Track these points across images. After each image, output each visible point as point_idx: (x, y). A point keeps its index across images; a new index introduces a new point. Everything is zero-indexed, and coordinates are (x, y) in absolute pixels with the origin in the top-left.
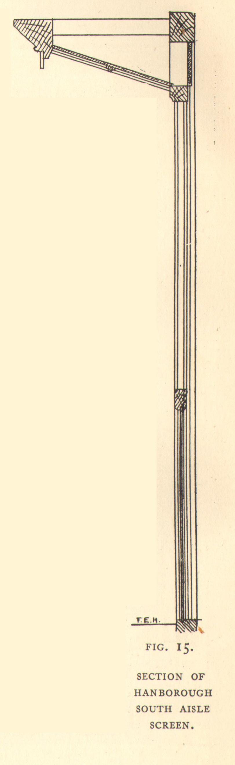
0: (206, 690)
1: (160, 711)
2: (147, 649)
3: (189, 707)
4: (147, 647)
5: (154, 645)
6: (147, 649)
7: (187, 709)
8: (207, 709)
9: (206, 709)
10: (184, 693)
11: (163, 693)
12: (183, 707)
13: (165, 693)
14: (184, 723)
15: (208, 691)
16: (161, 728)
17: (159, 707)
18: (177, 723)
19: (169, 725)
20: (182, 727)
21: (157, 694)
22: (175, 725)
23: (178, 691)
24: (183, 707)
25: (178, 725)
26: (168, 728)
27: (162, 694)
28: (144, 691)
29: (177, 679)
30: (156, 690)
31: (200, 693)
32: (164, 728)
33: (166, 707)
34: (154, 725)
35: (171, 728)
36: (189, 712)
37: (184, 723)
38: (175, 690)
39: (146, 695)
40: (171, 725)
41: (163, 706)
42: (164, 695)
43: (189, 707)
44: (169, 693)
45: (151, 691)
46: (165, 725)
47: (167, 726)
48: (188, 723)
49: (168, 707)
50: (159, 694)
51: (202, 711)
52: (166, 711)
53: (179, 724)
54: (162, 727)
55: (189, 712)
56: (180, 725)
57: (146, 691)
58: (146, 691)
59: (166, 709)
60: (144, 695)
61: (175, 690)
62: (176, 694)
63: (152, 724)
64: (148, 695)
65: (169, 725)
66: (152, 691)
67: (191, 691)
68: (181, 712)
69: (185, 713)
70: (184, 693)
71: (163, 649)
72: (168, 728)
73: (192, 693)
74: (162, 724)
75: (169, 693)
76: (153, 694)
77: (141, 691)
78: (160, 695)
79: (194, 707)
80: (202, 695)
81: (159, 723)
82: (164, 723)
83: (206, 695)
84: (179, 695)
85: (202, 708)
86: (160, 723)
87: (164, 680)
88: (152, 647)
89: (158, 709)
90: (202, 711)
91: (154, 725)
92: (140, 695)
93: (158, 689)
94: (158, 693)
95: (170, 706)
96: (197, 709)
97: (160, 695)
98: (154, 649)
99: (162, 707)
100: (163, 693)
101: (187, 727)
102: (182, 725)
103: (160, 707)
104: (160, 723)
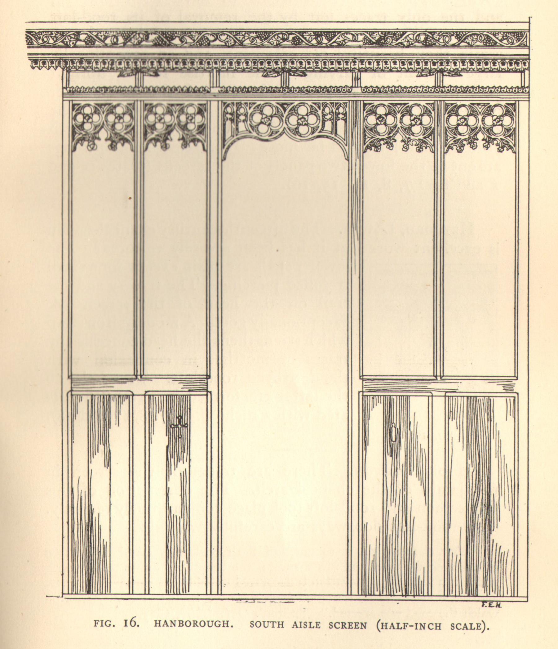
0: (224, 621)
1: (273, 627)
2: (95, 626)
3: (301, 622)
4: (95, 623)
5: (102, 621)
6: (95, 626)
7: (299, 625)
10: (202, 624)
11: (182, 623)
12: (295, 623)
13: (184, 623)
14: (362, 624)
15: (226, 622)
16: (339, 628)
17: (272, 623)
18: (355, 623)
19: (347, 626)
20: (360, 627)
21: (176, 625)
22: (353, 625)
23: (197, 622)
24: (295, 623)
25: (356, 625)
27: (181, 625)
28: (391, 624)
29: (425, 624)
30: (175, 621)
31: (217, 624)
32: (342, 628)
33: (279, 622)
34: (333, 625)
35: (349, 628)
36: (301, 627)
38: (194, 621)
39: (165, 625)
41: (276, 622)
42: (183, 625)
44: (188, 624)
46: (343, 625)
47: (346, 626)
48: (366, 623)
49: (281, 623)
51: (313, 627)
52: (279, 627)
53: (357, 624)
54: (341, 627)
55: (301, 627)
56: (99, 623)
57: (165, 621)
58: (165, 621)
59: (279, 625)
61: (194, 621)
65: (347, 626)
66: (171, 621)
67: (209, 622)
68: (293, 627)
70: (202, 624)
71: (110, 625)
73: (210, 624)
76: (172, 625)
77: (161, 622)
78: (180, 626)
80: (220, 625)
82: (342, 623)
83: (224, 626)
84: (197, 626)
87: (126, 619)
88: (100, 623)
89: (271, 624)
90: (313, 627)
91: (333, 625)
92: (160, 626)
94: (177, 624)
96: (308, 624)
97: (180, 626)
98: (102, 626)
99: (274, 623)
100: (182, 623)
102: (360, 625)
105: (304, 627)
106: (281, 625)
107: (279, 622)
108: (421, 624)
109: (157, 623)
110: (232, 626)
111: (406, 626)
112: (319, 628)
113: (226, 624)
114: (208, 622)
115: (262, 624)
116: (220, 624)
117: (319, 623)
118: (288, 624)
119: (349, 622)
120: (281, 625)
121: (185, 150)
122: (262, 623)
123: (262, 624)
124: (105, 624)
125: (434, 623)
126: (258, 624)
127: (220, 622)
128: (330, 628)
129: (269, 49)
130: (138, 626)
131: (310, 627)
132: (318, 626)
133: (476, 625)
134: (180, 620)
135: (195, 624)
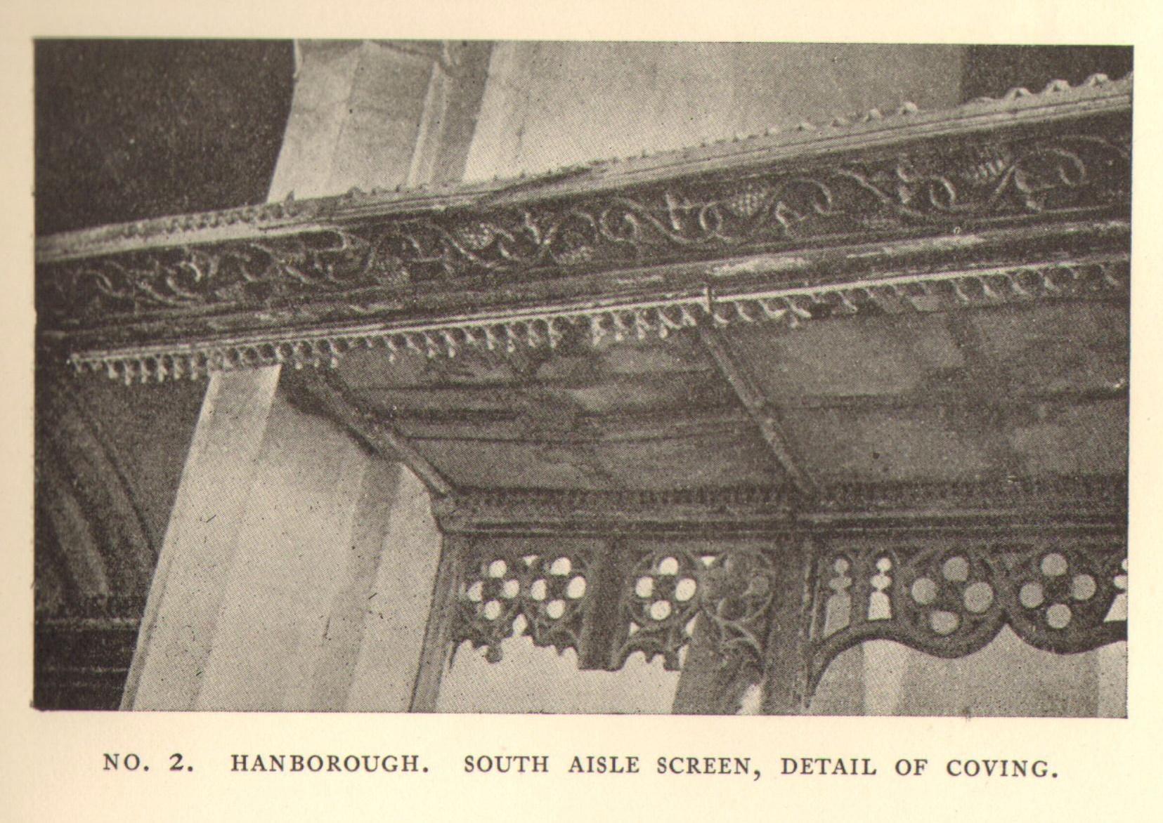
0: (405, 757)
3: (590, 759)
7: (585, 766)
8: (634, 764)
9: (630, 764)
10: (352, 764)
11: (300, 763)
12: (577, 759)
13: (305, 763)
14: (738, 761)
15: (410, 760)
17: (518, 760)
19: (701, 766)
20: (734, 770)
22: (717, 766)
23: (337, 759)
24: (577, 759)
26: (699, 772)
27: (298, 766)
28: (255, 758)
29: (117, 755)
30: (282, 757)
31: (389, 764)
32: (690, 772)
33: (535, 758)
34: (667, 764)
35: (707, 772)
36: (590, 770)
37: (738, 761)
38: (330, 757)
39: (258, 768)
40: (707, 765)
41: (528, 758)
42: (302, 767)
43: (590, 759)
44: (315, 764)
45: (271, 759)
46: (692, 766)
47: (698, 767)
48: (747, 759)
50: (291, 767)
51: (621, 771)
52: (535, 770)
54: (686, 769)
56: (729, 764)
57: (259, 758)
58: (259, 758)
59: (536, 764)
60: (254, 770)
61: (330, 757)
62: (333, 767)
63: (662, 761)
64: (263, 769)
65: (701, 766)
66: (274, 758)
68: (571, 771)
69: (264, 773)
70: (352, 764)
71: (1045, 773)
72: (699, 772)
73: (371, 765)
74: (686, 762)
75: (315, 764)
76: (276, 767)
77: (247, 759)
78: (294, 769)
79: (602, 761)
80: (395, 767)
81: (679, 761)
82: (690, 760)
84: (339, 769)
85: (622, 763)
86: (682, 760)
89: (516, 765)
90: (621, 771)
93: (288, 753)
94: (288, 763)
95: (545, 758)
96: (609, 764)
97: (294, 769)
99: (525, 760)
100: (300, 763)
101: (746, 770)
102: (732, 766)
103: (522, 758)
104: (682, 760)
105: (599, 771)
106: (541, 764)
107: (535, 758)
108: (1016, 763)
109: (239, 763)
110: (1055, 775)
111: (923, 767)
112: (637, 771)
113: (410, 763)
114: (366, 758)
115: (496, 763)
116: (395, 763)
117: (637, 759)
118: (558, 764)
119: (805, 757)
120: (541, 764)
121: (37, 714)
122: (362, 761)
123: (496, 763)
124: (134, 762)
125: (717, 757)
126: (485, 764)
127: (396, 759)
128: (659, 771)
129: (192, 713)
130: (146, 768)
131: (614, 770)
132: (633, 768)
133: (627, 761)
134: (331, 754)
135: (333, 763)
